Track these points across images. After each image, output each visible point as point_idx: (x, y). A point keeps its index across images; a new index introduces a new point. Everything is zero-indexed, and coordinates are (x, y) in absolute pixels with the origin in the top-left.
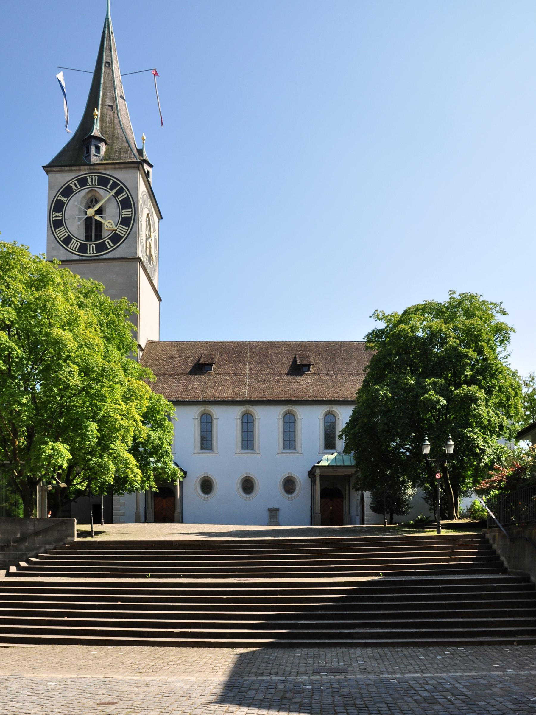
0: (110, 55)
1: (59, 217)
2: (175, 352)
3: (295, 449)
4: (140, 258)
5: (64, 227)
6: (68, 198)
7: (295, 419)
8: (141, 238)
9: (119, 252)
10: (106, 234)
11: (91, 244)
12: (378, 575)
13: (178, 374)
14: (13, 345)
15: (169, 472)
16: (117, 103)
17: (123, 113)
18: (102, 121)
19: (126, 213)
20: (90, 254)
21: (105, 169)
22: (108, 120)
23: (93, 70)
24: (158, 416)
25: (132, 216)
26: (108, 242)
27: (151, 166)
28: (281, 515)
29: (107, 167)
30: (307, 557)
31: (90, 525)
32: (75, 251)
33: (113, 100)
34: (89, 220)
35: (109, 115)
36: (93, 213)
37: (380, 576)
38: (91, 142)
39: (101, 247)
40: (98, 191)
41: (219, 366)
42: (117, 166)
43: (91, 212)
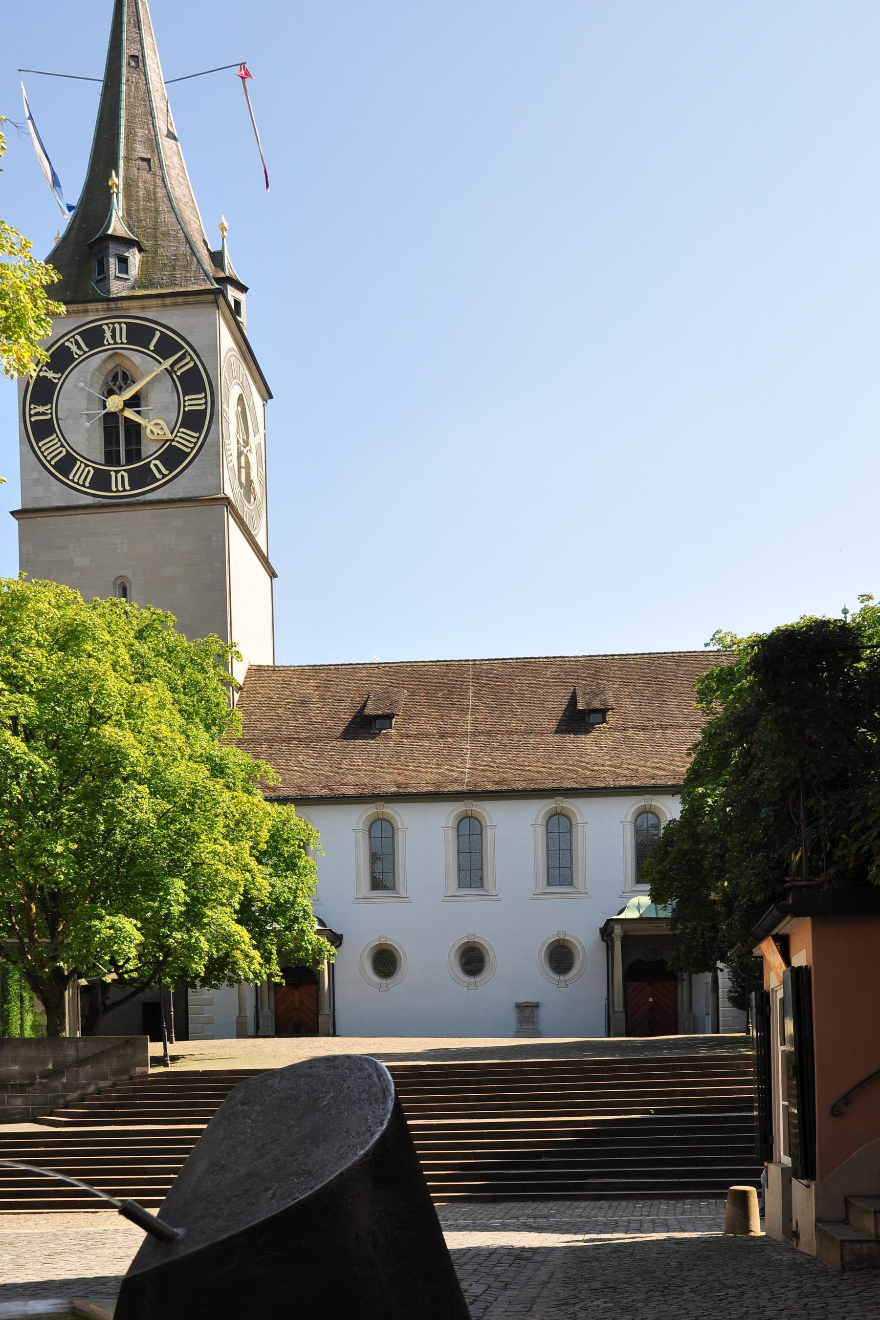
0: (138, 39)
1: (44, 414)
2: (309, 689)
3: (571, 884)
4: (227, 499)
5: (57, 436)
6: (62, 375)
7: (571, 825)
8: (229, 453)
9: (179, 488)
10: (150, 448)
11: (120, 471)
12: (647, 1112)
13: (319, 739)
14: (35, 758)
15: (310, 947)
16: (159, 153)
17: (173, 173)
18: (128, 196)
19: (194, 402)
20: (118, 491)
21: (143, 308)
22: (141, 193)
23: (101, 74)
24: (286, 849)
25: (206, 408)
26: (156, 465)
27: (243, 289)
28: (544, 1016)
29: (146, 302)
30: (540, 1089)
31: (162, 1043)
32: (83, 485)
33: (151, 145)
34: (111, 419)
35: (145, 182)
36: (121, 405)
37: (650, 1113)
38: (107, 248)
39: (141, 477)
40: (130, 357)
41: (409, 717)
42: (168, 301)
43: (115, 403)
